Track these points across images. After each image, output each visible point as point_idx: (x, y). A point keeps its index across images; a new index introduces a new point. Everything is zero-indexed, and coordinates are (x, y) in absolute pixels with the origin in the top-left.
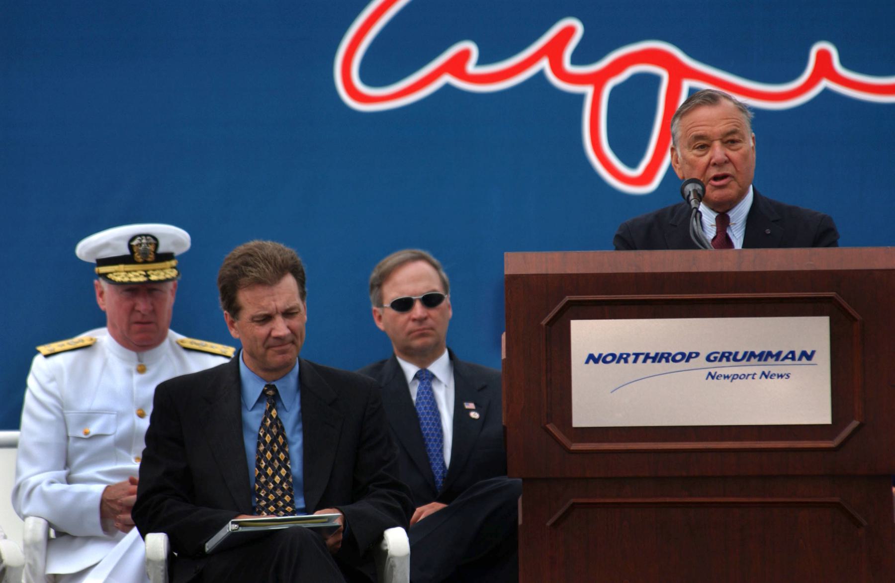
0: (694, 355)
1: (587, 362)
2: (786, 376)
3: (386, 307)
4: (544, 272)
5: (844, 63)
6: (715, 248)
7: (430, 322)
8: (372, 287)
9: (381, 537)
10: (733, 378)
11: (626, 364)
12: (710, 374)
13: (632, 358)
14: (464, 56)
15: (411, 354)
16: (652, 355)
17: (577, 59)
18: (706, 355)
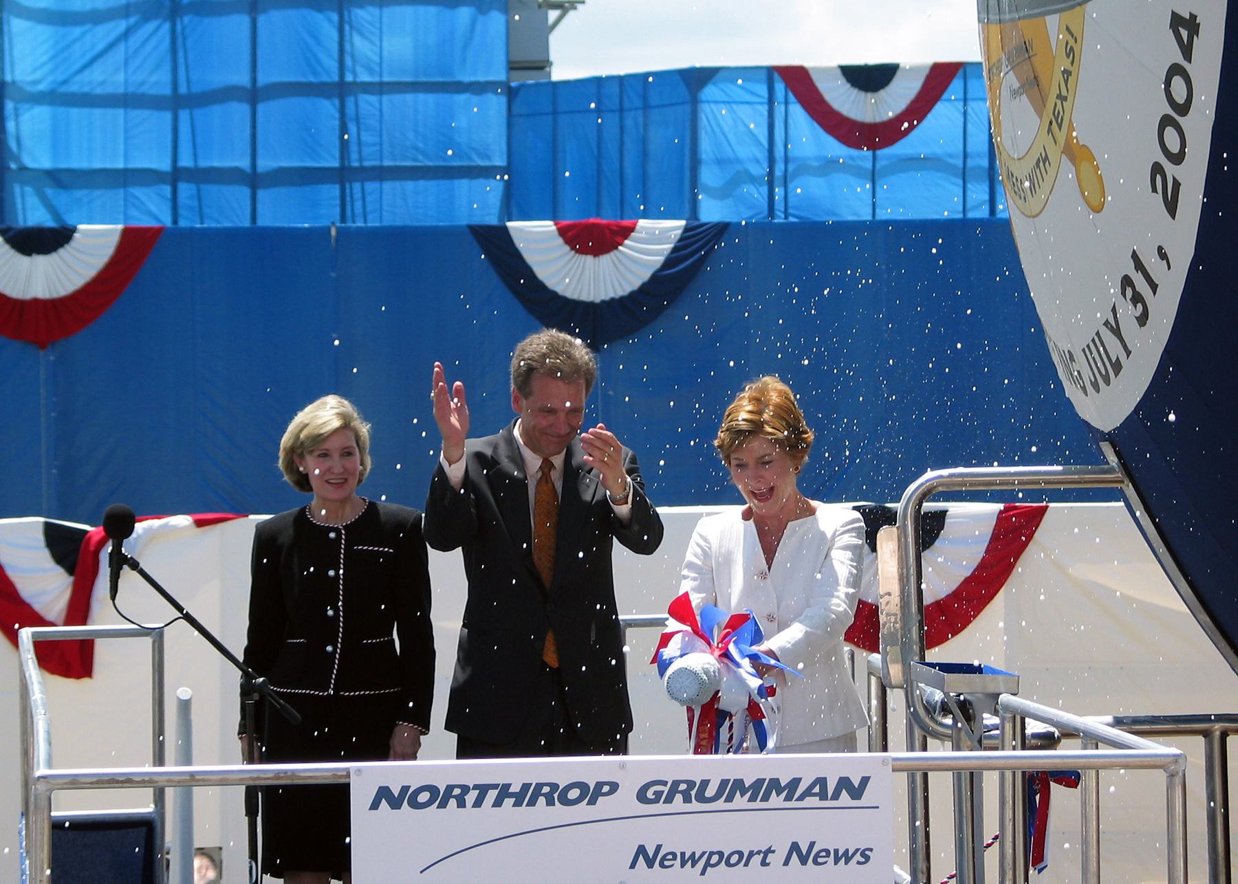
0: (606, 789)
2: (858, 857)
6: (666, 647)
10: (708, 864)
12: (641, 850)
13: (471, 797)
16: (515, 788)
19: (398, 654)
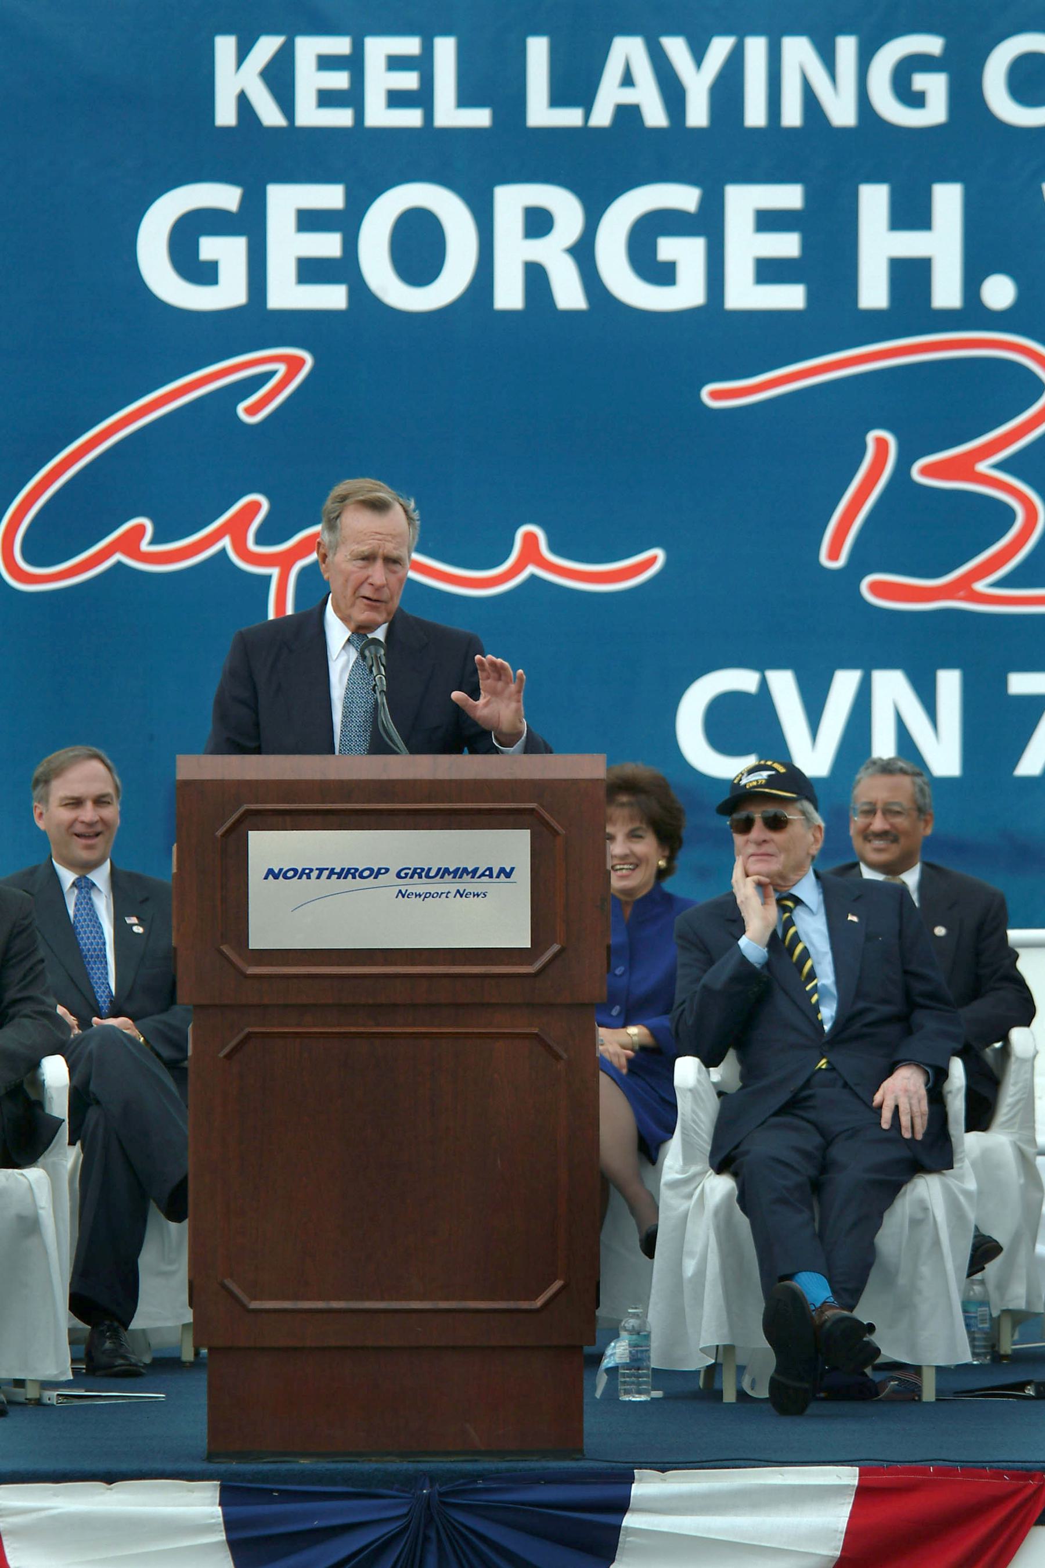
0: (383, 871)
4: (219, 777)
5: (553, 548)
8: (37, 782)
9: (36, 1065)
10: (425, 897)
13: (315, 874)
15: (71, 865)
16: (337, 870)
17: (261, 539)
19: (175, 845)
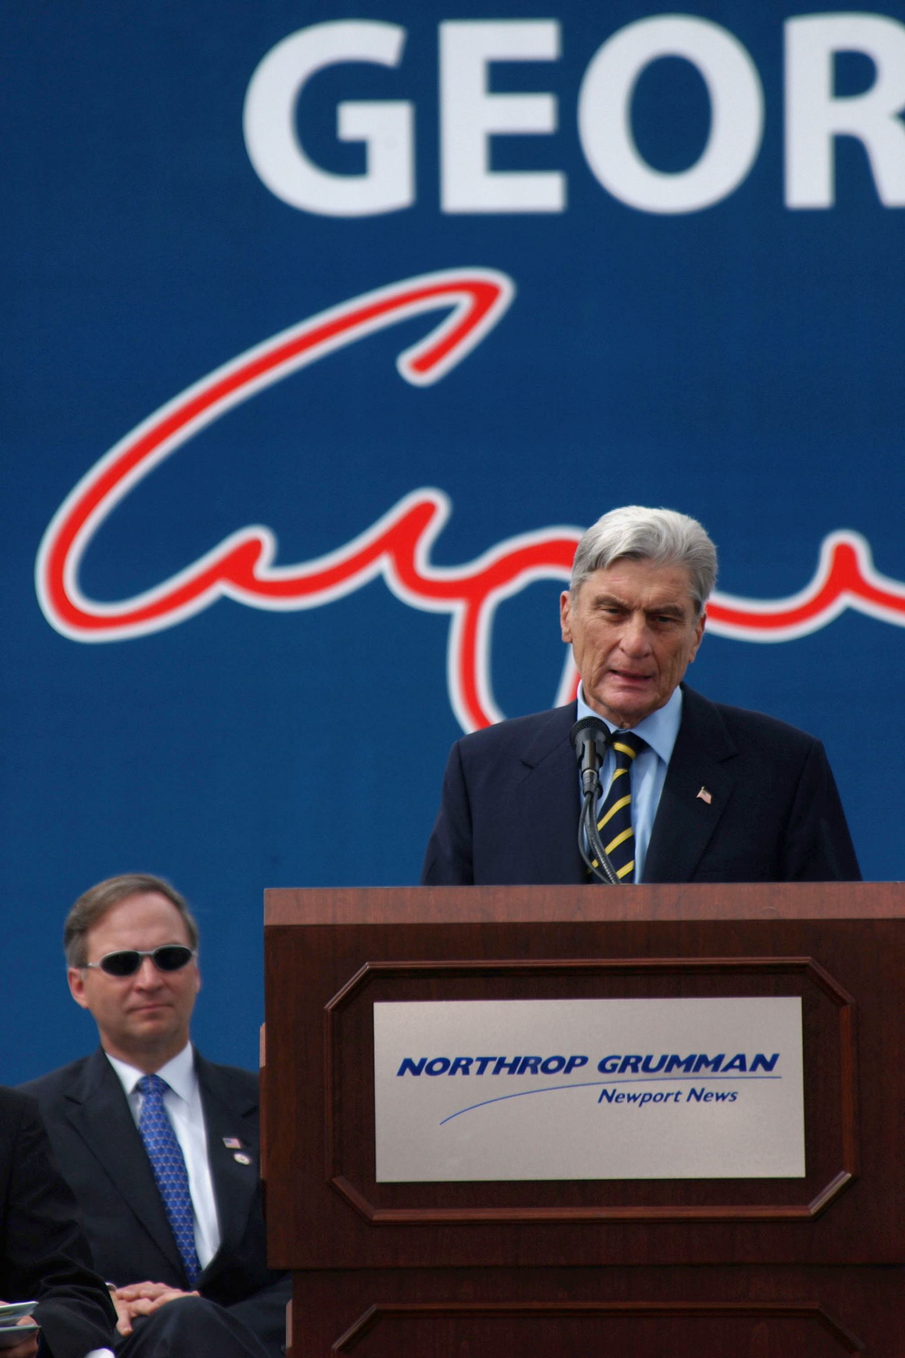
0: (578, 1061)
1: (401, 1072)
2: (730, 1097)
3: (92, 968)
4: (329, 921)
7: (167, 995)
8: (70, 934)
10: (643, 1101)
11: (466, 1077)
12: (605, 1092)
13: (475, 1067)
14: (253, 549)
16: (510, 1060)
18: (598, 1061)
